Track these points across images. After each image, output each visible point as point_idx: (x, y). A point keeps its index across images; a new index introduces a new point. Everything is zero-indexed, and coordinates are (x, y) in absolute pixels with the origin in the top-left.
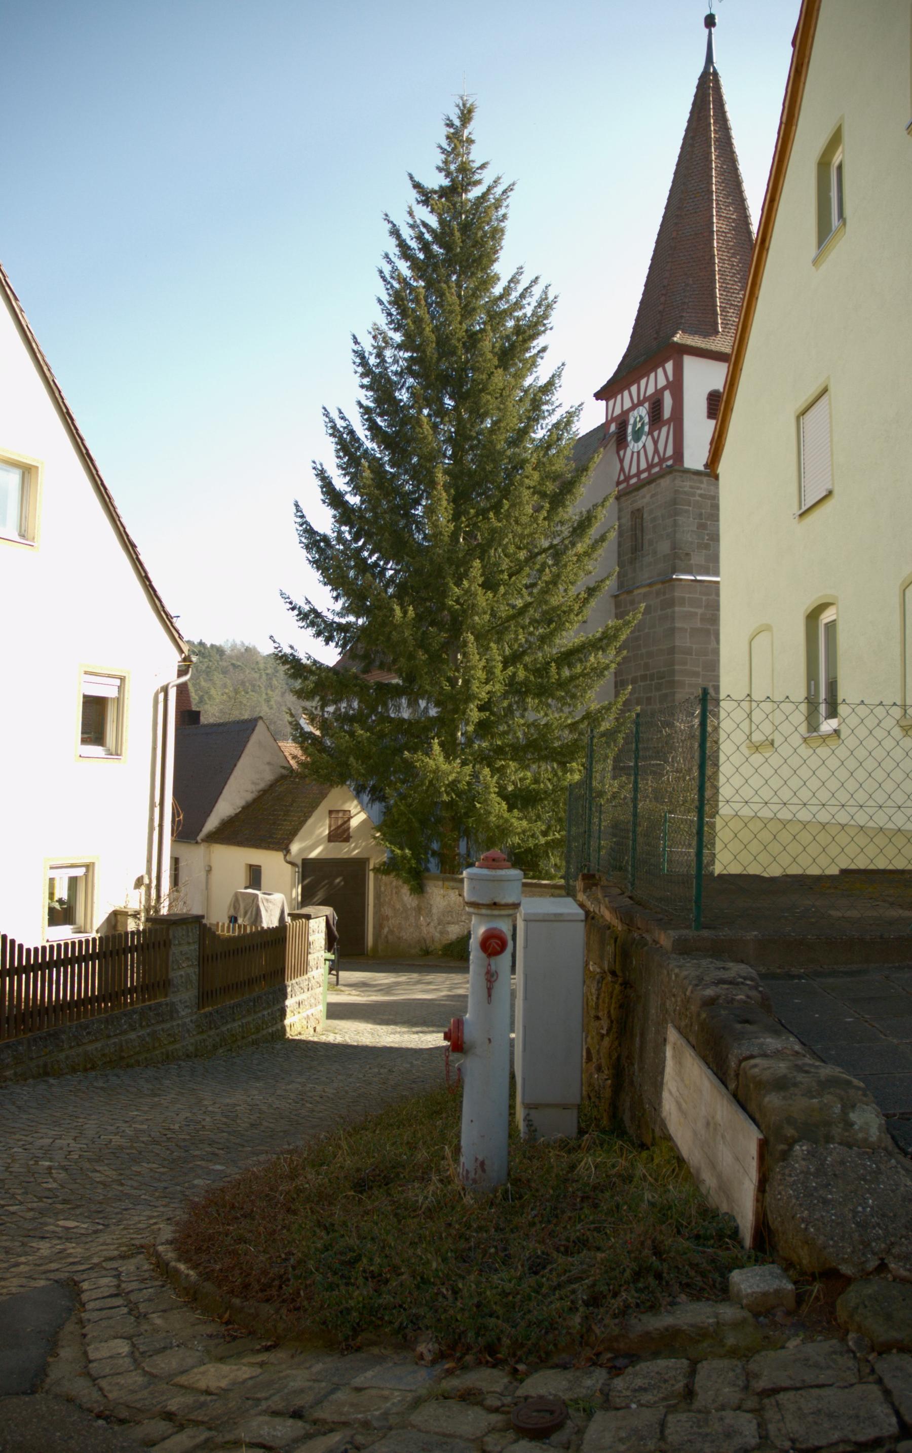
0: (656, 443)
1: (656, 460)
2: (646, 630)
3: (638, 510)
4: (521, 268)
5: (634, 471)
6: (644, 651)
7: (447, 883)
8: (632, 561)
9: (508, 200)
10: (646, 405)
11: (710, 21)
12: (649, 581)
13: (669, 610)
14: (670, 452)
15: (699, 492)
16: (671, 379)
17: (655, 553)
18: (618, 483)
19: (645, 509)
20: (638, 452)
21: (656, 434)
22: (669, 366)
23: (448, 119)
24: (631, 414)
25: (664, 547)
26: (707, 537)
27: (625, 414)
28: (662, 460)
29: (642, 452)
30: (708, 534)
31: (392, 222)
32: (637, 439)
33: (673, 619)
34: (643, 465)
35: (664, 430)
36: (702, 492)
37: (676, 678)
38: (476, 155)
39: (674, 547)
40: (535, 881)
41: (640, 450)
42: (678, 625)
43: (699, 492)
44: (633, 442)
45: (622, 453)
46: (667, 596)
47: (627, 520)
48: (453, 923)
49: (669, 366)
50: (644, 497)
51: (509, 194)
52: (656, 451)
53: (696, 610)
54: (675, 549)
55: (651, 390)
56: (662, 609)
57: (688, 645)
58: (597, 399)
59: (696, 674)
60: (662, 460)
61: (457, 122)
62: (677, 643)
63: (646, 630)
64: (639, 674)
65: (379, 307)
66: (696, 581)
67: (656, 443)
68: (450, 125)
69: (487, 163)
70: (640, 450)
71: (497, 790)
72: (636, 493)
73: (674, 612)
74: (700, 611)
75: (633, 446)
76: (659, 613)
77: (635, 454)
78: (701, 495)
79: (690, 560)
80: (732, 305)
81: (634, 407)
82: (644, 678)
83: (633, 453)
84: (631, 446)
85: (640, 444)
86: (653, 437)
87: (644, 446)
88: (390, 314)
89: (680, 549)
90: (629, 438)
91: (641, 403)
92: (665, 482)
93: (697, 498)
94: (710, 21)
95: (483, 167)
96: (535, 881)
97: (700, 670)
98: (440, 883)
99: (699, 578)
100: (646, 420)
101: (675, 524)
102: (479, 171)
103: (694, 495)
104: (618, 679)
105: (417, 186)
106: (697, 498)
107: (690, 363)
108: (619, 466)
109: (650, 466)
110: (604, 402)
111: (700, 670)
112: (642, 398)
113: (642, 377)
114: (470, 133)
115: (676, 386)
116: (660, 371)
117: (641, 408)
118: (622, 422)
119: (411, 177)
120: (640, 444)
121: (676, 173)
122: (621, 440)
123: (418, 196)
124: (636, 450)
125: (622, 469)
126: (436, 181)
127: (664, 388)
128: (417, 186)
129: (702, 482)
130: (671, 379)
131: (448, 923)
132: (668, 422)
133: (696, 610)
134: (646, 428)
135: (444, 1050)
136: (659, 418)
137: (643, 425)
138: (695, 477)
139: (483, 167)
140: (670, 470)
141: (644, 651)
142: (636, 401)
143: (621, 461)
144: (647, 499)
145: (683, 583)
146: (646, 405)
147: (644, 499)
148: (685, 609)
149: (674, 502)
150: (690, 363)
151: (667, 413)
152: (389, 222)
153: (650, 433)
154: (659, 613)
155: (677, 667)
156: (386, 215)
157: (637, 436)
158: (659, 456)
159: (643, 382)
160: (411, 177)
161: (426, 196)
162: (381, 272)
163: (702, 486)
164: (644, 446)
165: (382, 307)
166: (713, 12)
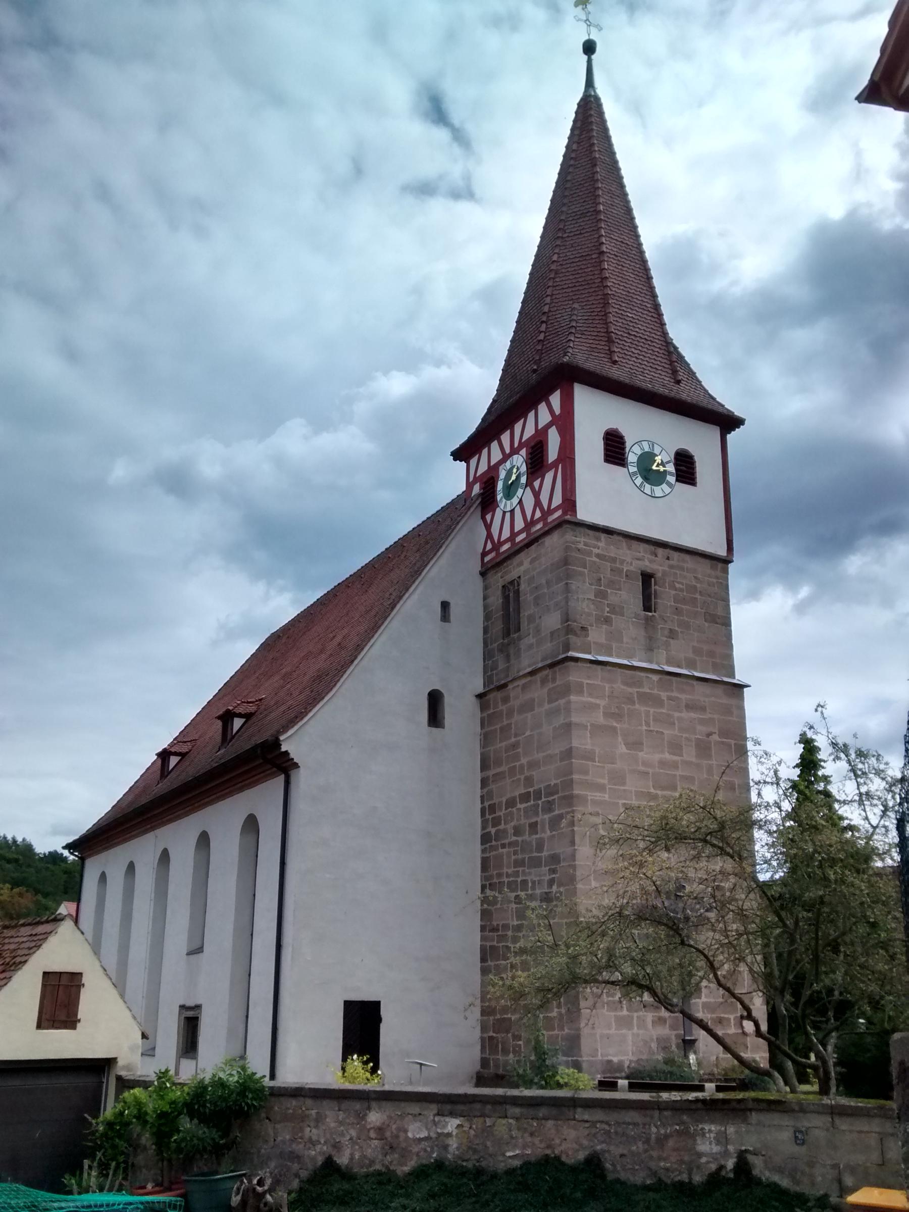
0: (537, 495)
1: (538, 514)
2: (528, 733)
3: (512, 583)
5: (506, 534)
6: (524, 761)
8: (503, 649)
10: (523, 452)
11: (589, 48)
12: (529, 670)
13: (562, 702)
14: (557, 500)
15: (596, 551)
16: (557, 411)
17: (538, 631)
18: (484, 554)
19: (522, 579)
20: (512, 512)
21: (537, 484)
22: (555, 399)
24: (501, 468)
25: (552, 621)
27: (493, 470)
29: (518, 511)
30: (608, 605)
32: (509, 495)
33: (568, 710)
34: (519, 524)
35: (549, 476)
37: (576, 792)
39: (566, 618)
40: (499, 1091)
41: (515, 509)
42: (575, 719)
43: (596, 551)
44: (504, 500)
45: (488, 517)
46: (558, 683)
47: (496, 600)
50: (521, 564)
52: (538, 503)
53: (598, 701)
54: (567, 621)
56: (550, 702)
57: (589, 747)
58: (455, 460)
59: (601, 788)
60: (546, 513)
62: (575, 743)
63: (528, 733)
64: (517, 794)
67: (537, 495)
70: (515, 509)
72: (509, 562)
73: (569, 702)
74: (602, 703)
75: (504, 505)
76: (547, 706)
77: (508, 515)
78: (598, 556)
79: (587, 636)
81: (506, 457)
82: (525, 797)
83: (504, 513)
84: (502, 506)
85: (515, 501)
86: (533, 489)
87: (520, 502)
89: (575, 621)
90: (499, 497)
91: (514, 451)
92: (553, 541)
93: (594, 559)
94: (589, 48)
96: (499, 1091)
97: (606, 781)
100: (524, 469)
101: (567, 589)
103: (590, 554)
104: (486, 804)
106: (594, 559)
108: (484, 533)
109: (529, 525)
110: (464, 464)
111: (606, 781)
112: (516, 445)
113: (517, 420)
115: (565, 422)
117: (515, 457)
118: (489, 482)
120: (515, 501)
121: (553, 201)
122: (487, 501)
124: (508, 509)
125: (489, 536)
129: (598, 539)
130: (557, 411)
132: (555, 464)
133: (598, 701)
134: (523, 480)
135: (720, 612)
136: (542, 462)
137: (518, 477)
138: (591, 532)
140: (559, 524)
141: (524, 761)
142: (508, 451)
143: (488, 527)
144: (526, 565)
146: (523, 452)
147: (521, 567)
148: (584, 699)
149: (566, 562)
151: (552, 454)
153: (529, 483)
154: (547, 706)
155: (575, 777)
157: (510, 491)
158: (542, 509)
159: (518, 427)
163: (600, 544)
164: (520, 502)
166: (592, 37)
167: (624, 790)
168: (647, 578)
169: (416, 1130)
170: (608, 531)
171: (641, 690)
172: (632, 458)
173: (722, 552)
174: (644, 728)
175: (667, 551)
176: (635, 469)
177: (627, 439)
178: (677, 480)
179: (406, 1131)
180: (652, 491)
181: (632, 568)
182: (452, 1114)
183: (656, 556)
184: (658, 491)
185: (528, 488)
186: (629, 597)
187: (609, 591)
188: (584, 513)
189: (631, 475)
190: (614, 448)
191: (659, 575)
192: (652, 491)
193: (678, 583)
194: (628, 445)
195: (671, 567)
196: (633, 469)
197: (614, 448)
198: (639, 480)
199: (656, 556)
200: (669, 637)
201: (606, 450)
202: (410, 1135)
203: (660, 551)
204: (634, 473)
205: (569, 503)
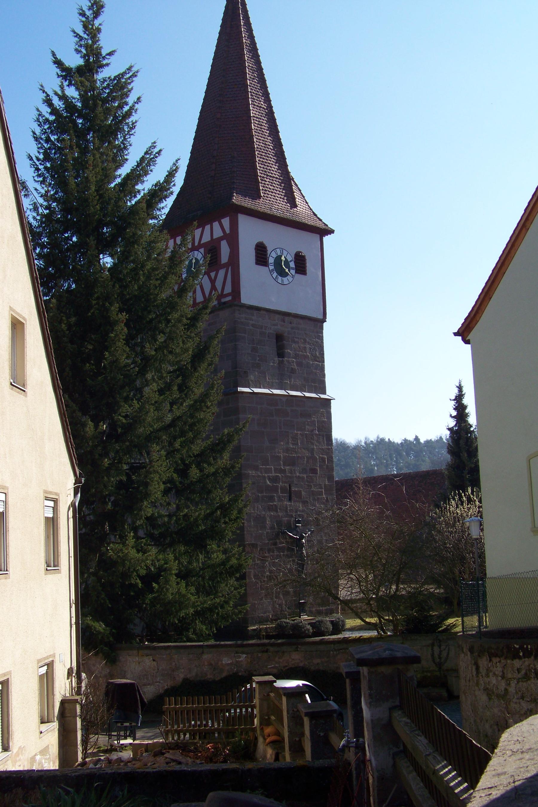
4: (155, 143)
7: (141, 652)
9: (132, 85)
10: (202, 250)
14: (228, 289)
16: (228, 231)
22: (226, 222)
23: (82, 10)
26: (258, 359)
28: (222, 295)
31: (46, 93)
35: (222, 273)
36: (254, 322)
38: (106, 43)
43: (251, 322)
48: (149, 684)
49: (226, 222)
51: (134, 79)
52: (213, 288)
55: (206, 238)
61: (88, 13)
65: (29, 162)
66: (254, 393)
67: (213, 282)
68: (83, 14)
69: (114, 51)
71: (177, 572)
78: (253, 325)
80: (267, 175)
86: (210, 277)
88: (38, 169)
95: (111, 54)
98: (135, 652)
99: (256, 390)
102: (108, 57)
105: (58, 63)
107: (243, 221)
112: (196, 244)
114: (100, 25)
115: (232, 238)
116: (216, 225)
119: (54, 54)
123: (58, 71)
126: (74, 61)
127: (220, 239)
128: (58, 63)
130: (228, 231)
131: (144, 685)
132: (226, 266)
134: (203, 269)
139: (111, 54)
145: (244, 395)
150: (243, 221)
152: (44, 92)
153: (207, 273)
156: (42, 86)
160: (54, 54)
161: (67, 74)
162: (34, 133)
165: (31, 162)
167: (479, 601)
168: (279, 338)
169: (226, 660)
170: (258, 309)
171: (277, 408)
172: (271, 260)
173: (321, 317)
174: (278, 430)
175: (291, 318)
176: (273, 267)
177: (268, 249)
178: (296, 272)
179: (222, 661)
180: (282, 281)
181: (271, 331)
182: (243, 653)
183: (284, 322)
184: (285, 279)
185: (206, 276)
186: (270, 349)
187: (259, 347)
188: (245, 300)
189: (271, 272)
190: (261, 254)
191: (286, 334)
192: (282, 281)
193: (296, 338)
194: (269, 252)
195: (292, 328)
196: (271, 267)
197: (261, 254)
198: (275, 275)
199: (284, 322)
200: (291, 373)
201: (257, 257)
202: (223, 662)
203: (287, 319)
204: (273, 270)
205: (236, 291)
